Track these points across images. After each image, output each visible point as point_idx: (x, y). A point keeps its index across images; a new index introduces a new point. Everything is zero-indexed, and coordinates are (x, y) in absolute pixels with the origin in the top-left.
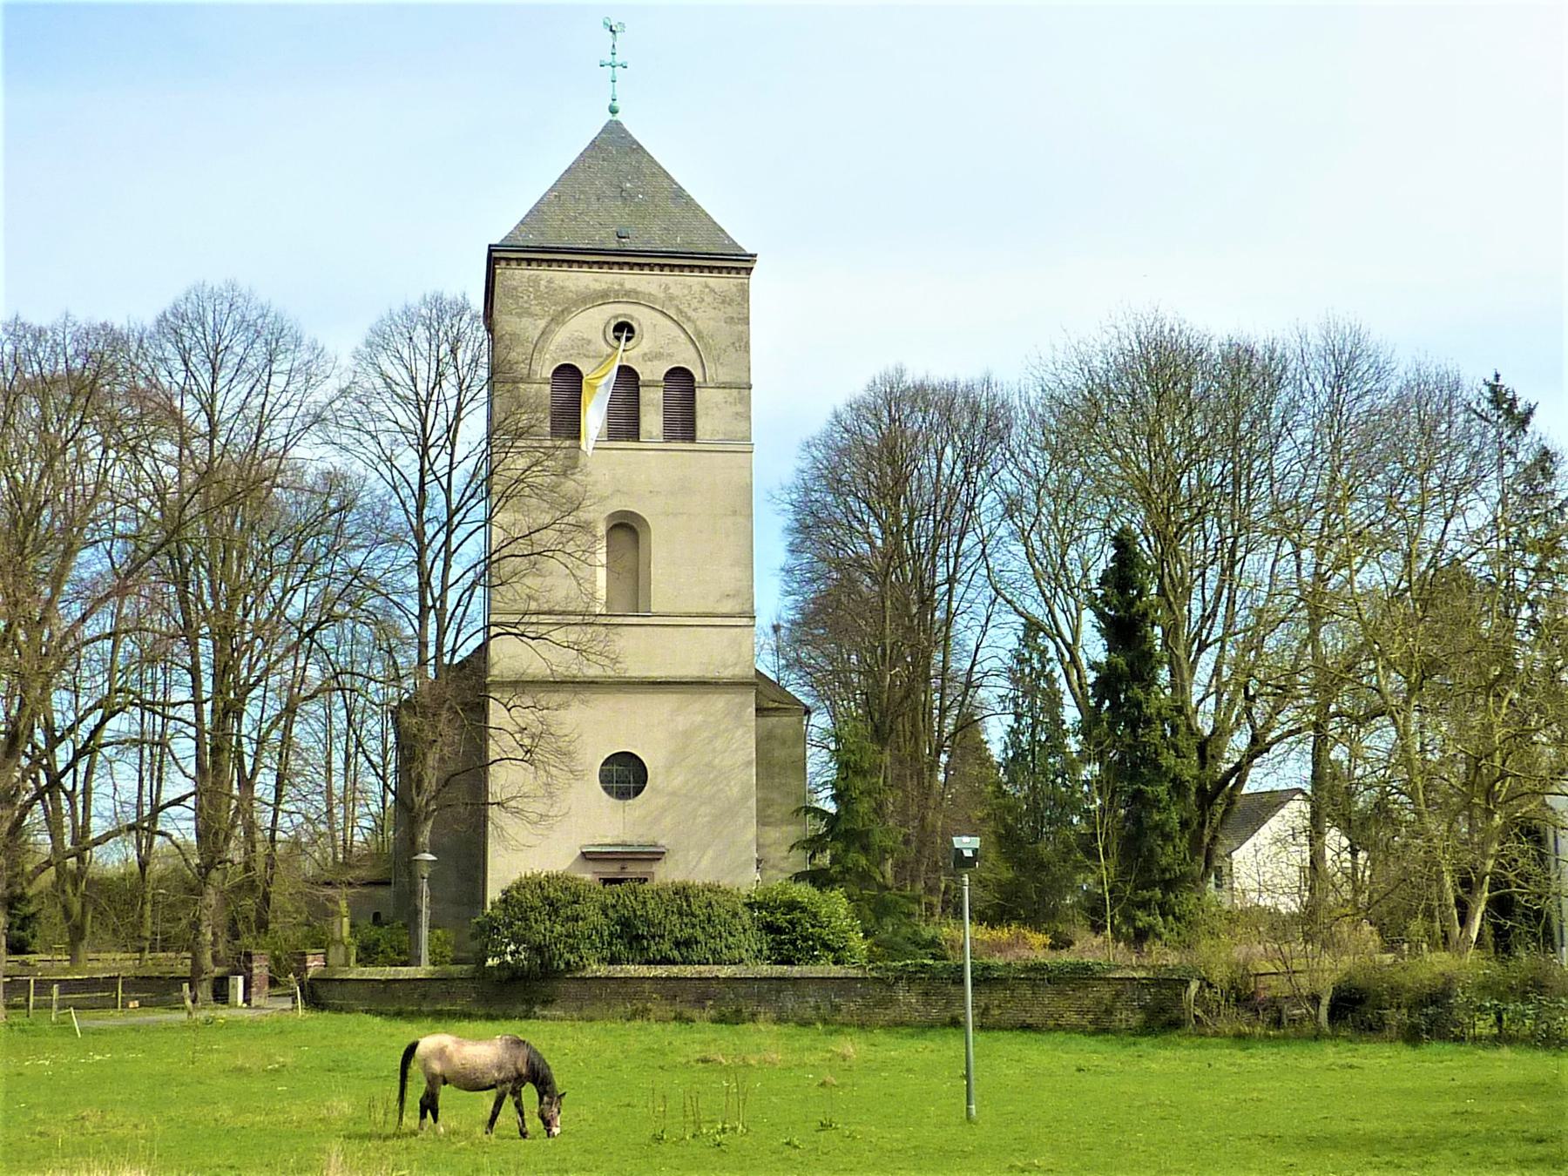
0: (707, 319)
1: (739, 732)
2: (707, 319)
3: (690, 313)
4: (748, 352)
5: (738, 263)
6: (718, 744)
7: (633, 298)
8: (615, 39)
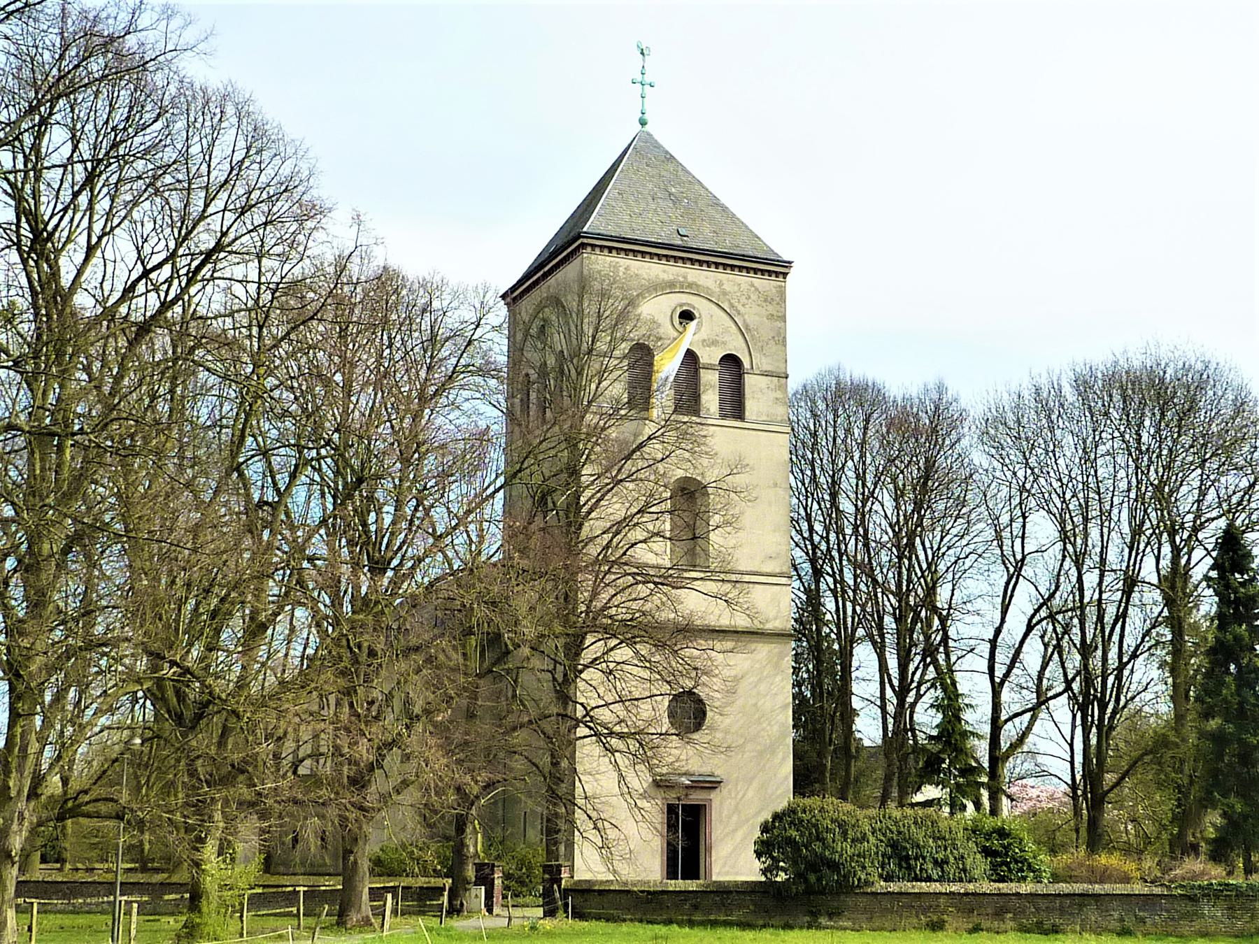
0: (753, 314)
1: (779, 678)
2: (753, 314)
3: (740, 308)
4: (785, 346)
5: (776, 268)
6: (763, 687)
7: (693, 289)
8: (644, 60)
